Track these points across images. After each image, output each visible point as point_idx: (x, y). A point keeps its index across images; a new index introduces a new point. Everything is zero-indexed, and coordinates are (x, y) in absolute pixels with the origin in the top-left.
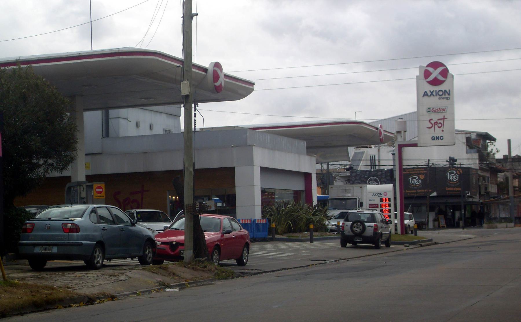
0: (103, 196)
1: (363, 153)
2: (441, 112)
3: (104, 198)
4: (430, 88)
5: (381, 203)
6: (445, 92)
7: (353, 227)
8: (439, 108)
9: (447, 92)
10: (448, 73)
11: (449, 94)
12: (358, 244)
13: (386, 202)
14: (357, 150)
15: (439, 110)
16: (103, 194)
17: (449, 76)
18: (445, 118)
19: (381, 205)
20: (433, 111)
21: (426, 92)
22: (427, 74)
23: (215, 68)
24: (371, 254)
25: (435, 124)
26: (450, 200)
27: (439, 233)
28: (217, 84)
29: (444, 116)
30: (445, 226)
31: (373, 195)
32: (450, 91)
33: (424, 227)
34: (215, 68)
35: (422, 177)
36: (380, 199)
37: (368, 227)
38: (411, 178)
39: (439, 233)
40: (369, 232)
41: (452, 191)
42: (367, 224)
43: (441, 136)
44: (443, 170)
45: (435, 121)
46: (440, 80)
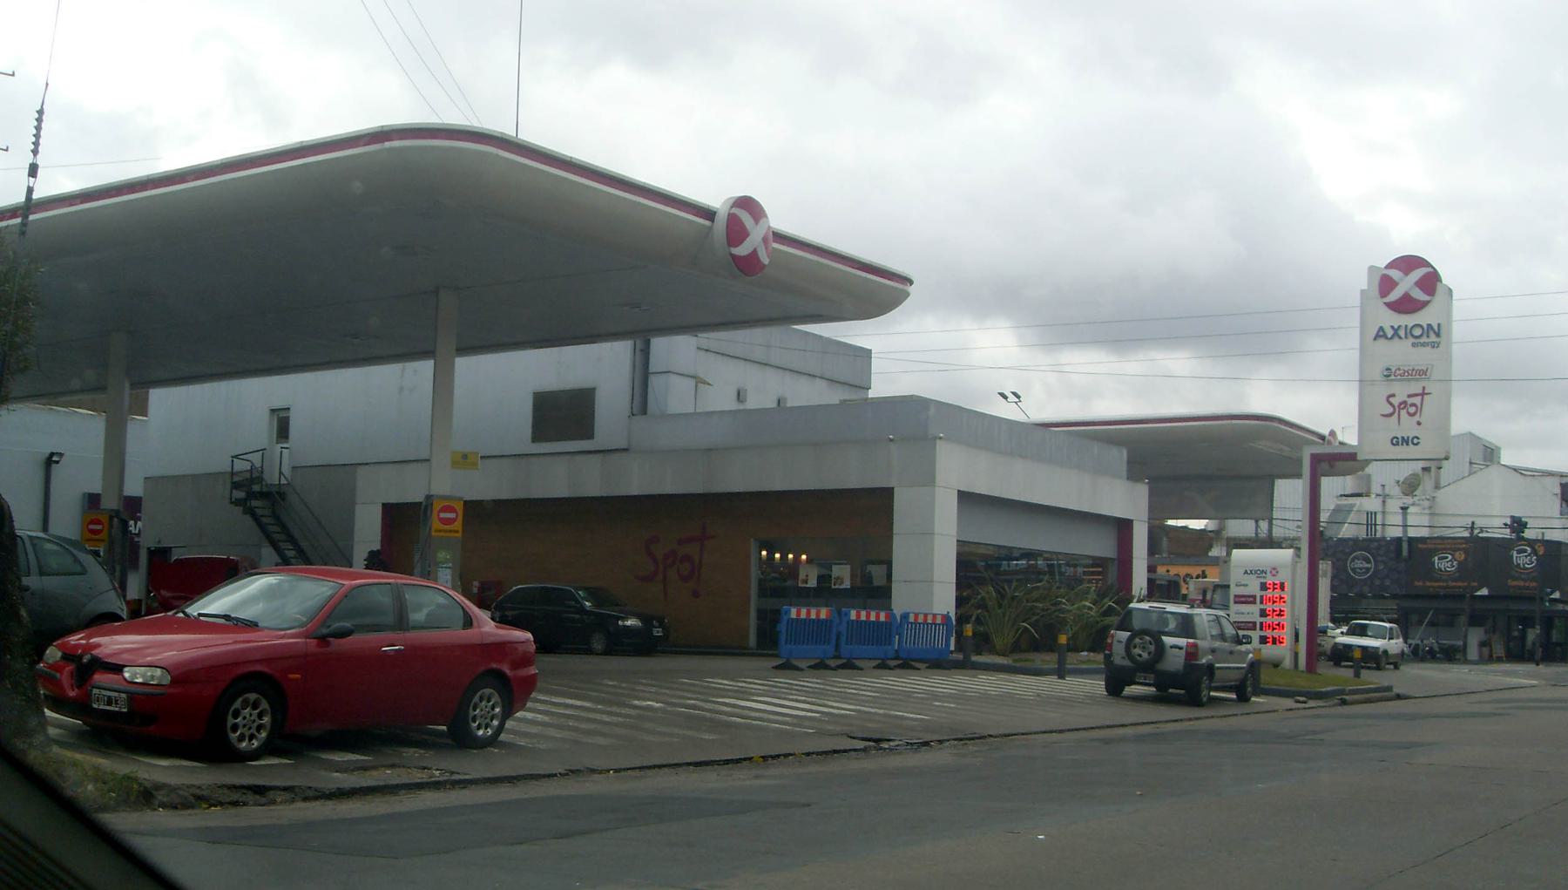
0: (457, 532)
1: (1353, 506)
2: (1418, 377)
3: (459, 535)
4: (1391, 319)
5: (1263, 593)
6: (1428, 330)
7: (1132, 645)
8: (1411, 368)
9: (1435, 332)
10: (1439, 283)
11: (1438, 335)
12: (1170, 690)
14: (1340, 500)
16: (458, 525)
17: (1439, 289)
18: (1426, 392)
19: (1262, 597)
21: (1381, 329)
22: (1386, 284)
23: (734, 210)
24: (1097, 730)
25: (1402, 406)
26: (1514, 606)
27: (1470, 671)
28: (742, 250)
29: (1424, 388)
30: (1502, 657)
31: (1246, 572)
33: (1457, 657)
34: (734, 210)
35: (1461, 556)
36: (1261, 583)
37: (1171, 647)
38: (1436, 558)
39: (1470, 671)
40: (1174, 661)
41: (1519, 588)
42: (1168, 640)
43: (1414, 435)
44: (1503, 546)
45: (1401, 400)
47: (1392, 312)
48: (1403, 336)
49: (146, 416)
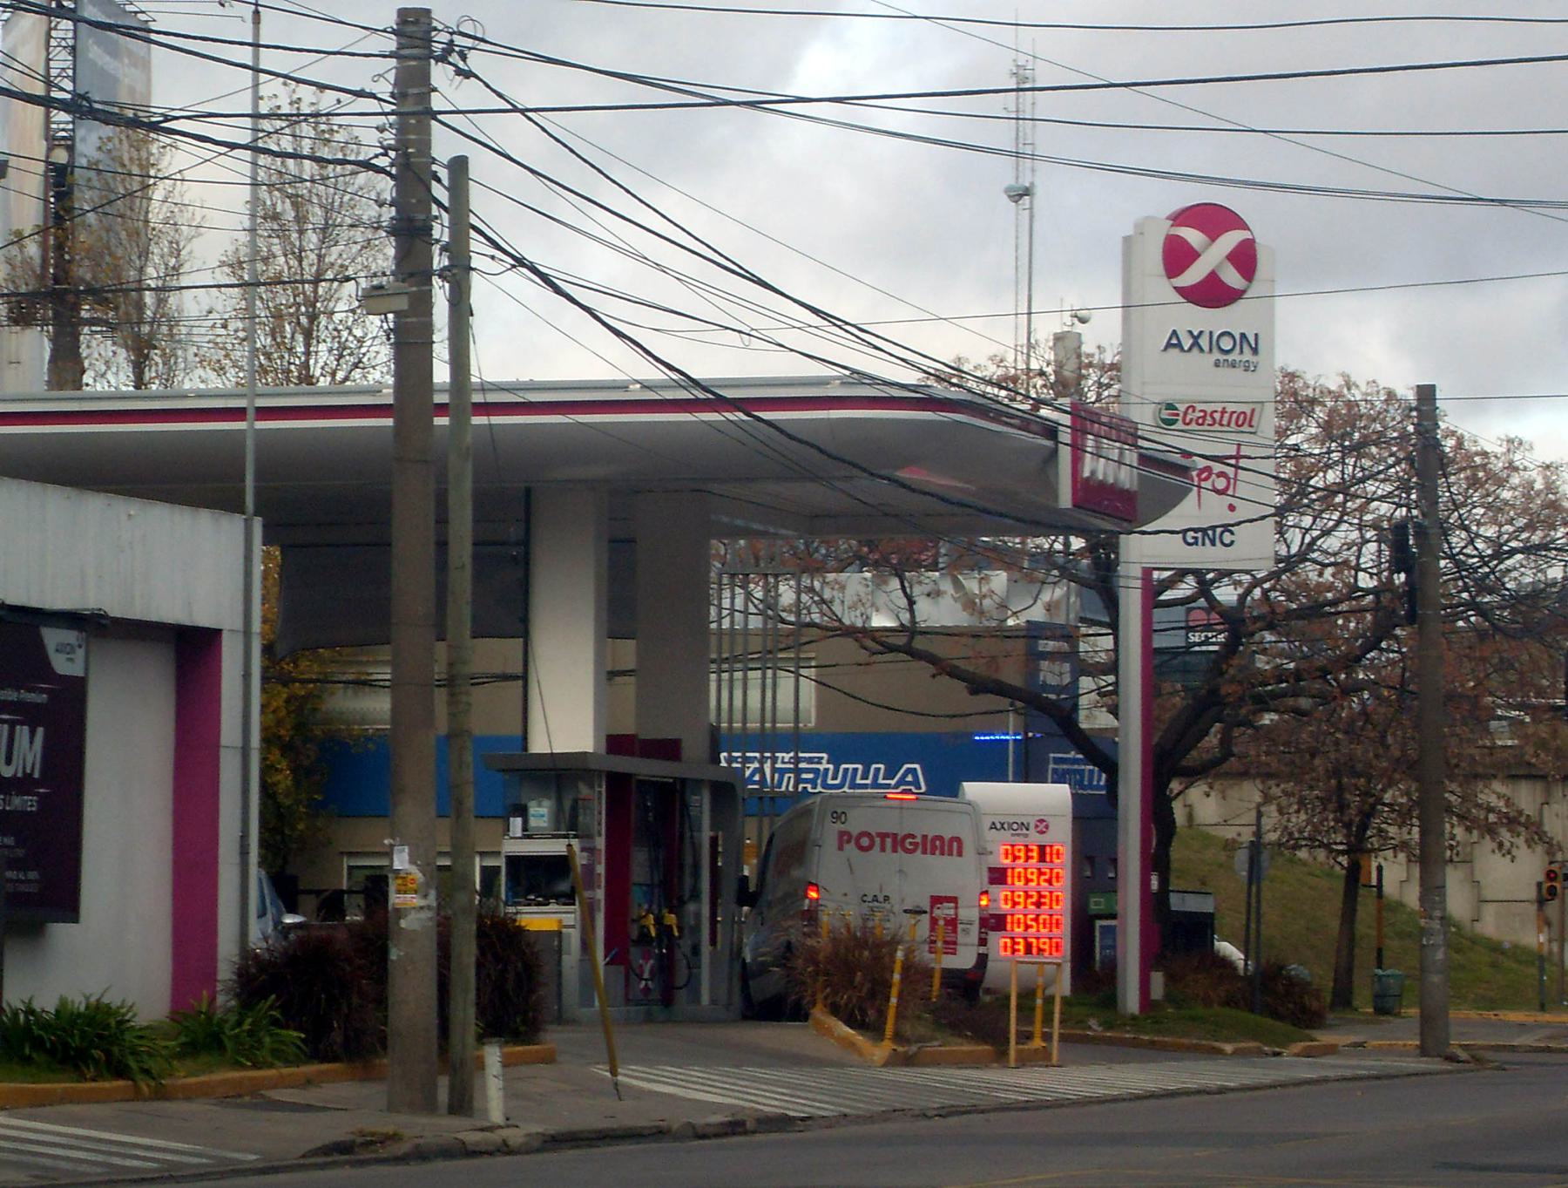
6: (1241, 342)
8: (1219, 407)
11: (1255, 351)
13: (1026, 861)
15: (1222, 417)
20: (1187, 421)
22: (1177, 257)
25: (1204, 476)
32: (1260, 337)
46: (53, 669)
47: (1227, 308)
48: (1206, 348)
49: (1011, 974)
